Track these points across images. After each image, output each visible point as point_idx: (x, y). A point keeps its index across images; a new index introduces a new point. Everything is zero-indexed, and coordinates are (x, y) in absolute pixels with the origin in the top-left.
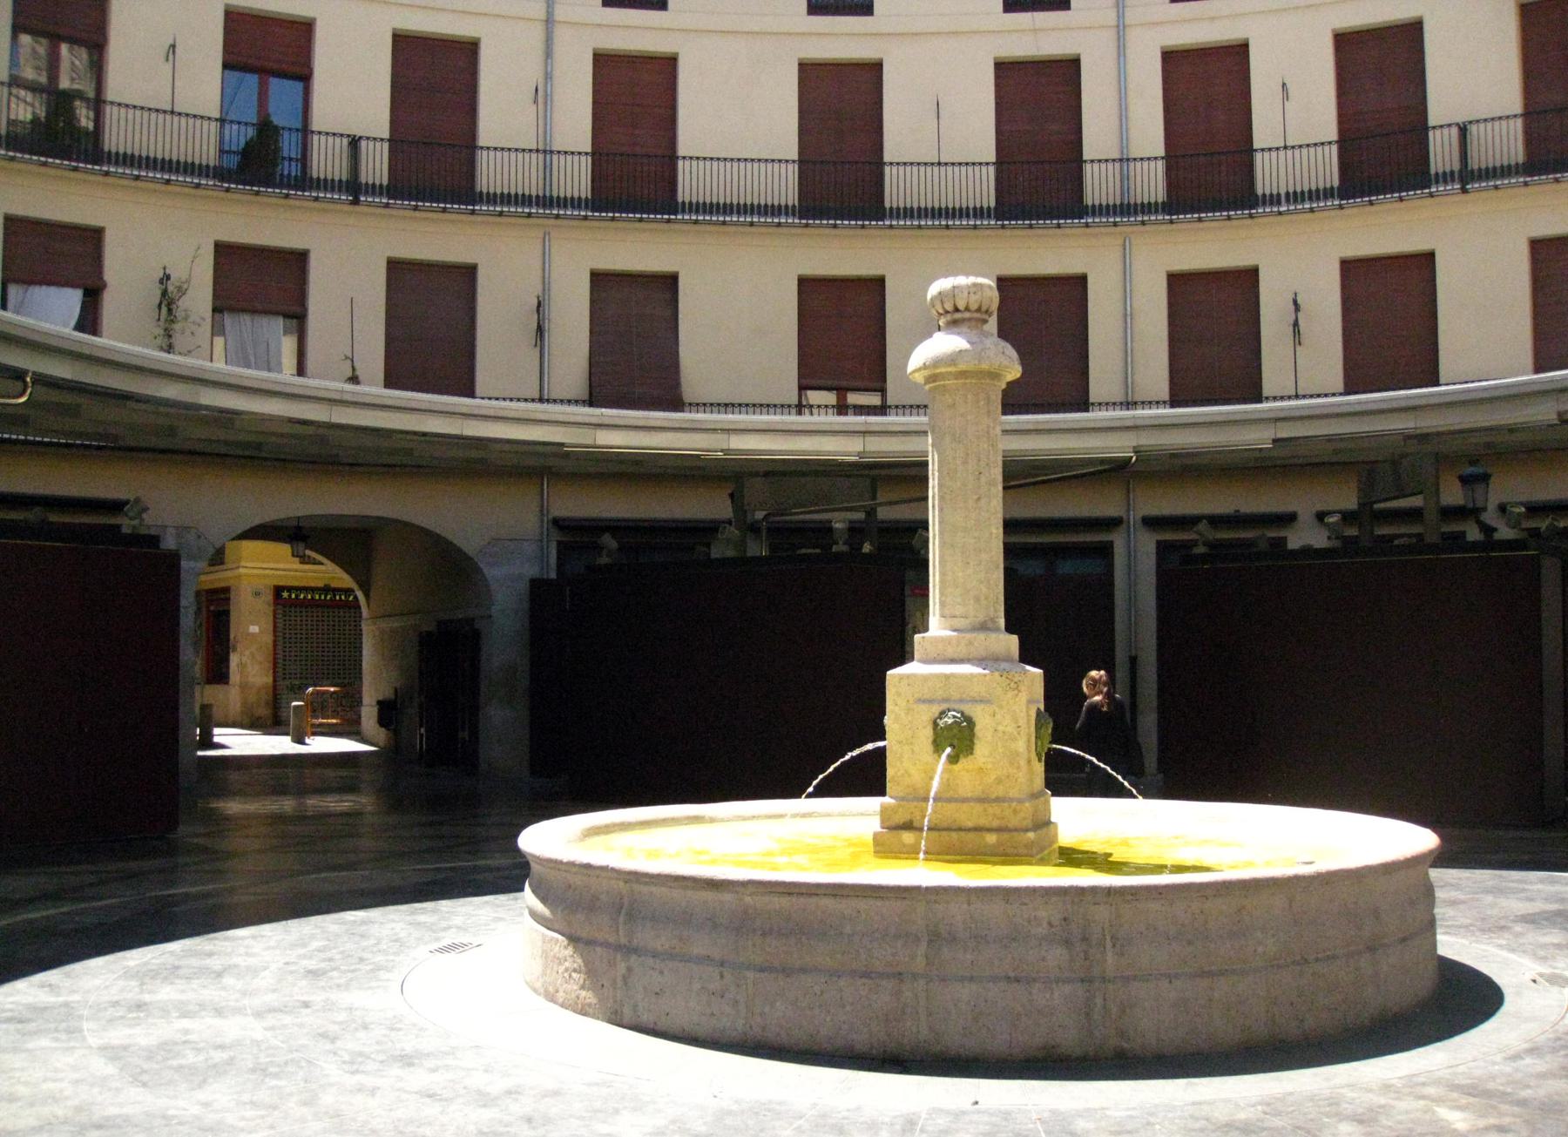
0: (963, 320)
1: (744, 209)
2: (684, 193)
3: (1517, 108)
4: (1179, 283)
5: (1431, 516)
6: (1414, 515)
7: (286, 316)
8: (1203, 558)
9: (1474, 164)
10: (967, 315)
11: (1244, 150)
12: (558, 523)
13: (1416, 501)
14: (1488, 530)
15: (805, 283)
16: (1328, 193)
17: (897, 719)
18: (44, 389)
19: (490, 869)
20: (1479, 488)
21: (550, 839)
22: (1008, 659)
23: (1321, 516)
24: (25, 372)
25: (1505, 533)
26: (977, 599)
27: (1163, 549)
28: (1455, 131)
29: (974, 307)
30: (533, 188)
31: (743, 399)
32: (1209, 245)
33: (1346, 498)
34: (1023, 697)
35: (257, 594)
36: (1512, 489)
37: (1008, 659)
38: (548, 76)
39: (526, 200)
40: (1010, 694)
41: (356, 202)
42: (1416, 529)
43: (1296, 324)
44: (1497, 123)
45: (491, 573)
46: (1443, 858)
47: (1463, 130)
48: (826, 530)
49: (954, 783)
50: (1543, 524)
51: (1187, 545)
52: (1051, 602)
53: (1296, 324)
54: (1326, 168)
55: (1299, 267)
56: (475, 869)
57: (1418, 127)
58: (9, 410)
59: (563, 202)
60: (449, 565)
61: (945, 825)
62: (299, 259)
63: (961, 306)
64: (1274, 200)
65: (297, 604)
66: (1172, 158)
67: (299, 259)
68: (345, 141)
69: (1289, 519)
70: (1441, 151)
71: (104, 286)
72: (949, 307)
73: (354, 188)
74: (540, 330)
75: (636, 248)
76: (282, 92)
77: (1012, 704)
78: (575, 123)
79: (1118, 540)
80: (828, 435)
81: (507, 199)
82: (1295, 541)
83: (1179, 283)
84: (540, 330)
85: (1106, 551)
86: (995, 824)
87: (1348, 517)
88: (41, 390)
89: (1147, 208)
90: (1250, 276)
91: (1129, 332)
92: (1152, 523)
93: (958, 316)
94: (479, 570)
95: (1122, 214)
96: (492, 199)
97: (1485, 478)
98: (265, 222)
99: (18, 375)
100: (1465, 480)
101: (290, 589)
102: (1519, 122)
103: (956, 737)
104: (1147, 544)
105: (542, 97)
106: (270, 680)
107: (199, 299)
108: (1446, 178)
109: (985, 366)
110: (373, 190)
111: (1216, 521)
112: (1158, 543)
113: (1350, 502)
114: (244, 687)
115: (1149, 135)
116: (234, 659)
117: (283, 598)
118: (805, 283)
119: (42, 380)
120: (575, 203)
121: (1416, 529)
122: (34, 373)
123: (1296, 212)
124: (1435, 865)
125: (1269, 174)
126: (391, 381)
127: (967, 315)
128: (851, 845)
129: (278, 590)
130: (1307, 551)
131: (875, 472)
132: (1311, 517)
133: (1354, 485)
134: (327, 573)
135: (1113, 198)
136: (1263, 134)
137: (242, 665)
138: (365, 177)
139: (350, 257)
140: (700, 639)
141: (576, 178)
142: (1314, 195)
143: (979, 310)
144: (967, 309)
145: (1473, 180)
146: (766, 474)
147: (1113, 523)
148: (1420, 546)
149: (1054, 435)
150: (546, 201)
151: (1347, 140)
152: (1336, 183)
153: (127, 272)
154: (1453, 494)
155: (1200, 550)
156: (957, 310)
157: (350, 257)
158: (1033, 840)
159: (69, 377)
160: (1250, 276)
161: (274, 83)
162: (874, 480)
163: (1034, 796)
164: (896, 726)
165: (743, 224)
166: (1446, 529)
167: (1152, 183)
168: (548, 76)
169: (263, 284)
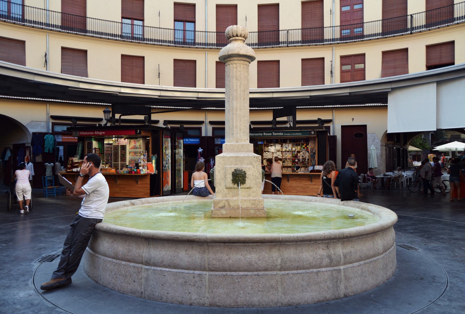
0: (239, 40)
12: (53, 117)
15: (303, 60)
17: (219, 172)
19: (334, 229)
26: (244, 132)
27: (214, 129)
28: (286, 31)
29: (243, 35)
39: (41, 24)
44: (373, 23)
50: (169, 126)
55: (332, 57)
56: (336, 229)
70: (282, 38)
74: (46, 61)
76: (189, 26)
79: (203, 127)
84: (46, 61)
85: (200, 129)
92: (211, 123)
94: (27, 129)
102: (381, 22)
104: (210, 128)
108: (283, 43)
112: (213, 128)
118: (303, 60)
126: (175, 85)
127: (240, 38)
128: (406, 230)
133: (272, 114)
141: (57, 20)
147: (202, 123)
161: (187, 24)
164: (218, 174)
165: (360, 41)
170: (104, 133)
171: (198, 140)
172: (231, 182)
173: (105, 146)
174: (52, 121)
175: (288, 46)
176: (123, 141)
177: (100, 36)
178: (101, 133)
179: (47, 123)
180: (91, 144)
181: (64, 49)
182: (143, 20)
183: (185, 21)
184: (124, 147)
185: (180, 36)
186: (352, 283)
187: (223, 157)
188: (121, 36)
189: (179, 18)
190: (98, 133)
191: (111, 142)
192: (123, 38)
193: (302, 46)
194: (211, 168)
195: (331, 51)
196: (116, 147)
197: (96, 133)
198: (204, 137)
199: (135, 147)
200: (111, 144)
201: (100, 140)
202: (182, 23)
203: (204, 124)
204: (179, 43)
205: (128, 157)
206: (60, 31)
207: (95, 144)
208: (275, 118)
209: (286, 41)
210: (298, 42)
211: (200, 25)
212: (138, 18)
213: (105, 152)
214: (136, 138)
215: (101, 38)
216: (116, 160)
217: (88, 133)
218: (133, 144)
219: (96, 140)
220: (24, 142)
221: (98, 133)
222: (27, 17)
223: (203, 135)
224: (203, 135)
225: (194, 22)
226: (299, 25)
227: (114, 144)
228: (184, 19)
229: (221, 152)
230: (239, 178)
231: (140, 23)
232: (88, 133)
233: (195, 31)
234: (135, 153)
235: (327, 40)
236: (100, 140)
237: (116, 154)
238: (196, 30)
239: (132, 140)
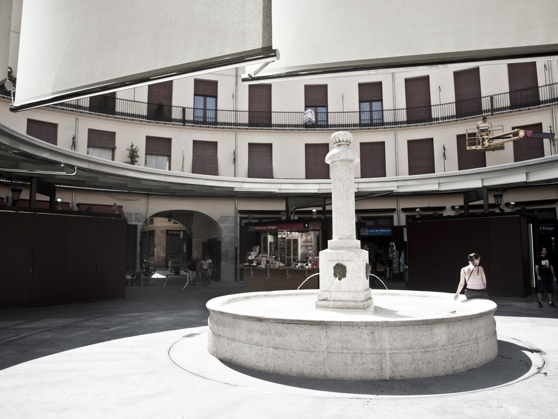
0: (342, 145)
1: (290, 126)
2: (274, 122)
3: (508, 91)
4: (411, 143)
5: (486, 206)
6: (480, 206)
7: (168, 156)
8: (418, 219)
9: (496, 106)
10: (343, 143)
11: (428, 106)
12: (241, 212)
13: (481, 202)
14: (502, 210)
16: (453, 117)
18: (81, 171)
20: (499, 199)
21: (213, 304)
22: (357, 248)
23: (453, 208)
24: (75, 166)
25: (507, 210)
26: (347, 229)
27: (407, 217)
28: (489, 98)
29: (345, 140)
30: (233, 121)
31: (289, 177)
32: (419, 133)
33: (459, 202)
34: (362, 259)
35: (162, 232)
36: (512, 199)
37: (357, 248)
38: (236, 91)
39: (230, 124)
40: (357, 258)
41: (184, 125)
42: (482, 211)
43: (444, 154)
45: (221, 225)
46: (498, 312)
47: (492, 98)
48: (311, 212)
49: (343, 284)
51: (414, 216)
52: (374, 230)
53: (444, 154)
54: (452, 110)
57: (479, 98)
58: (69, 178)
59: (241, 125)
60: (209, 223)
61: (337, 299)
62: (169, 140)
63: (341, 140)
64: (437, 119)
65: (173, 235)
66: (408, 109)
67: (169, 140)
68: (181, 109)
69: (443, 208)
70: (485, 104)
71: (115, 148)
72: (338, 141)
73: (184, 121)
74: (235, 160)
75: (260, 137)
77: (358, 260)
78: (244, 104)
80: (313, 187)
81: (225, 124)
82: (445, 214)
83: (411, 143)
84: (235, 160)
85: (392, 218)
86: (353, 299)
87: (461, 207)
88: (80, 172)
89: (402, 123)
90: (431, 140)
91: (397, 155)
92: (404, 210)
93: (340, 143)
95: (394, 125)
96: (221, 124)
97: (501, 196)
98: (160, 131)
99: (72, 167)
100: (495, 196)
101: (171, 231)
103: (340, 271)
104: (403, 216)
105: (235, 97)
106: (165, 255)
107: (142, 152)
109: (348, 158)
110: (189, 122)
111: (422, 209)
112: (406, 216)
113: (462, 203)
114: (158, 257)
115: (402, 103)
116: (156, 250)
117: (169, 234)
119: (79, 168)
120: (244, 125)
121: (482, 211)
122: (78, 167)
123: (444, 122)
124: (495, 315)
125: (436, 113)
127: (343, 143)
129: (167, 231)
130: (449, 217)
131: (324, 196)
132: (450, 208)
134: (179, 226)
135: (391, 120)
136: (434, 100)
137: (158, 251)
138: (187, 118)
139: (183, 141)
140: (270, 242)
141: (244, 118)
142: (449, 117)
143: (346, 141)
144: (343, 141)
145: (495, 111)
146: (295, 197)
147: (393, 210)
148: (483, 214)
149: (374, 185)
150: (236, 124)
151: (458, 102)
152: (455, 114)
153: (122, 145)
154: (492, 201)
155: (418, 217)
156: (340, 141)
157: (183, 141)
158: (364, 305)
159: (87, 167)
160: (431, 140)
162: (325, 198)
163: (366, 290)
166: (490, 210)
167: (403, 116)
168: (236, 91)
169: (159, 147)
170: (276, 227)
171: (390, 231)
172: (333, 275)
173: (279, 240)
174: (239, 215)
175: (492, 115)
176: (295, 235)
177: (283, 127)
178: (273, 228)
179: (235, 217)
180: (266, 238)
181: (251, 145)
182: (326, 106)
183: (371, 101)
184: (296, 241)
185: (366, 117)
186: (400, 368)
187: (326, 253)
188: (360, 125)
189: (365, 99)
190: (271, 228)
191: (284, 236)
192: (308, 126)
193: (511, 112)
194: (480, 265)
195: (550, 115)
196: (289, 241)
197: (268, 227)
198: (397, 227)
199: (306, 241)
200: (285, 238)
201: (275, 234)
202: (368, 103)
203: (396, 212)
204: (364, 125)
205: (300, 251)
206: (247, 129)
207: (270, 239)
208: (466, 202)
209: (490, 108)
210: (505, 108)
211: (387, 104)
212: (321, 105)
213: (279, 246)
214: (308, 231)
215: (285, 130)
216: (289, 255)
217: (262, 228)
218: (304, 238)
219: (271, 234)
220: (216, 237)
221: (271, 228)
222: (219, 120)
223: (396, 224)
224: (396, 224)
225: (381, 101)
226: (506, 88)
227: (287, 238)
228: (370, 99)
229: (327, 248)
230: (340, 271)
231: (323, 110)
232: (262, 228)
233: (382, 110)
234: (307, 247)
235: (543, 102)
236: (275, 234)
237: (289, 248)
238: (218, 108)
239: (304, 234)
